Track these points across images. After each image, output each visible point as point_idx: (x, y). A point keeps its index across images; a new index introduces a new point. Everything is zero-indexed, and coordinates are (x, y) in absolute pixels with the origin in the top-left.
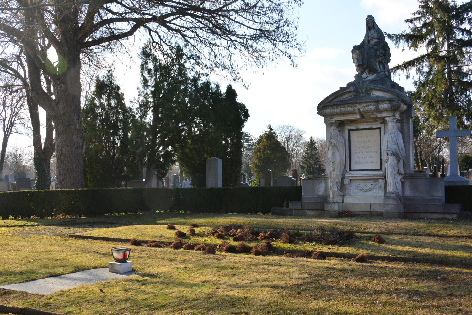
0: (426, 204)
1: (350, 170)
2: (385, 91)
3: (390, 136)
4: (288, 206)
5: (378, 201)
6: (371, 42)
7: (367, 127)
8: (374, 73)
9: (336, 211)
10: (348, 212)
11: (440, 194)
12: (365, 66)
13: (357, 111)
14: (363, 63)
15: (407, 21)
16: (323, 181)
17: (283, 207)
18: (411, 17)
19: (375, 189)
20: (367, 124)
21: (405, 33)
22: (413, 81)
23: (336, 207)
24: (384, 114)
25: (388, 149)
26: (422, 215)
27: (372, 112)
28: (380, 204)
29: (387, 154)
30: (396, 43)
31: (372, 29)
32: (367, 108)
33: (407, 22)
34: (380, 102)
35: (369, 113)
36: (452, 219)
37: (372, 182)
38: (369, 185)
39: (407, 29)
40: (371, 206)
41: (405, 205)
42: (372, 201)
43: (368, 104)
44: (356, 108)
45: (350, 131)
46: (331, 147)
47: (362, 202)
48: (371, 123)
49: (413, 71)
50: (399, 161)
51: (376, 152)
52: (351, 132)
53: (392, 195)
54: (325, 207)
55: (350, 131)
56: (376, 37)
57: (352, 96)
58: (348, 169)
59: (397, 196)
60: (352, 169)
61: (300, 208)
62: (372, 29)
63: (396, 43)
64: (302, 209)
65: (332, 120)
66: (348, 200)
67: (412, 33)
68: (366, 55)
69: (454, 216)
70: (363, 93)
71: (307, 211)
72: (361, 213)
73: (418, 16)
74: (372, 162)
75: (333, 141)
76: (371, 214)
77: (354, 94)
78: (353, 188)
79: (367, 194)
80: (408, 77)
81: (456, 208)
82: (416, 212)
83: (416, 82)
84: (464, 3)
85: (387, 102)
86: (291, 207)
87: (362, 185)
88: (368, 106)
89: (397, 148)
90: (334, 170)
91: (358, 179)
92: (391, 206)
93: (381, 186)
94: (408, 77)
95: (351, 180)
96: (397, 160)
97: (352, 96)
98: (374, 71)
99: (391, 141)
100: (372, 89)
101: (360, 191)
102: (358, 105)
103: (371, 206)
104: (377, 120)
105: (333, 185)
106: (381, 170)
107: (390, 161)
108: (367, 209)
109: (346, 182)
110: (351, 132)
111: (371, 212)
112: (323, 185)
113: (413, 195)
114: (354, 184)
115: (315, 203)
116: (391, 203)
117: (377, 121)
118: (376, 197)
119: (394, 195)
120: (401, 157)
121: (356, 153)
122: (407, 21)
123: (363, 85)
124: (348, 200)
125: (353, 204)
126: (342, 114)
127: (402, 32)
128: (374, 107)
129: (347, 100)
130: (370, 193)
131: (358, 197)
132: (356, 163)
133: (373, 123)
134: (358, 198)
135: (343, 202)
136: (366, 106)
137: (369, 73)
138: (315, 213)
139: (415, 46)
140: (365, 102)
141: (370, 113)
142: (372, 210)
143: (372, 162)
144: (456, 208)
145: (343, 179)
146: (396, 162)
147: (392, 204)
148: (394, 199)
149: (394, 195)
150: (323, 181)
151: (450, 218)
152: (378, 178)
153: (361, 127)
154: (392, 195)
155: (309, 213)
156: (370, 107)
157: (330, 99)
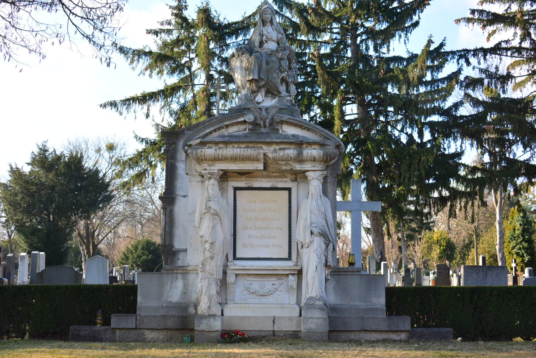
0: (362, 317)
1: (235, 258)
2: (305, 128)
3: (314, 203)
4: (107, 322)
5: (286, 313)
6: (265, 45)
7: (268, 185)
8: (274, 96)
9: (217, 331)
10: (237, 332)
11: (381, 301)
12: (263, 83)
13: (262, 156)
14: (259, 77)
15: (149, 32)
16: (180, 276)
17: (95, 324)
18: (157, 27)
19: (278, 293)
20: (268, 179)
21: (147, 50)
22: (154, 123)
23: (217, 325)
24: (307, 166)
25: (313, 225)
26: (353, 336)
27: (287, 160)
28: (290, 319)
29: (312, 233)
30: (132, 62)
31: (268, 24)
32: (281, 153)
33: (149, 33)
34: (305, 146)
35: (280, 162)
36: (400, 341)
37: (274, 280)
38: (268, 284)
39: (153, 44)
40: (274, 322)
41: (331, 320)
42: (277, 313)
43: (283, 146)
44: (262, 151)
46: (207, 215)
47: (259, 314)
48: (275, 179)
49: (156, 107)
50: (327, 246)
51: (281, 229)
52: (238, 192)
53: (318, 303)
54: (196, 325)
55: (236, 189)
56: (275, 38)
57: (245, 130)
58: (231, 257)
59: (325, 304)
60: (238, 256)
61: (134, 326)
62: (268, 24)
63: (132, 62)
64: (136, 328)
65: (212, 168)
66: (231, 311)
67: (159, 52)
68: (264, 63)
69: (403, 336)
70: (265, 126)
71: (147, 332)
72: (256, 334)
73: (167, 27)
74: (273, 245)
75: (212, 204)
76: (274, 335)
77: (250, 127)
78: (238, 289)
79: (264, 300)
80: (148, 116)
81: (405, 323)
82: (345, 331)
83: (157, 125)
84: (230, 22)
85: (316, 147)
86: (114, 324)
87: (256, 284)
88: (284, 149)
89: (325, 224)
90: (212, 258)
91: (249, 275)
92: (316, 321)
93: (291, 287)
94: (148, 116)
95: (236, 275)
96: (325, 243)
97: (245, 130)
98: (276, 93)
99: (316, 212)
100: (282, 122)
101: (252, 296)
102: (264, 147)
103: (274, 322)
104: (286, 174)
105: (209, 284)
106: (289, 258)
107: (315, 245)
108: (268, 327)
109: (231, 278)
110: (238, 192)
111: (274, 331)
112: (180, 283)
113: (340, 303)
114: (243, 282)
115: (164, 316)
116: (316, 316)
117: (286, 177)
118: (282, 306)
119: (321, 303)
120: (331, 239)
121: (245, 228)
122: (149, 32)
123: (267, 113)
124: (231, 311)
125: (243, 318)
126: (234, 159)
127: (142, 48)
128: (295, 152)
129: (236, 136)
130: (270, 299)
131: (251, 305)
132: (244, 246)
133: (280, 179)
134: (248, 308)
135: (222, 315)
136: (280, 149)
137: (266, 96)
138: (161, 335)
139: (454, 58)
140: (278, 143)
141: (283, 163)
142: (276, 329)
143: (273, 245)
144: (405, 323)
145: (225, 273)
146: (324, 246)
147: (318, 318)
148: (322, 309)
149: (321, 303)
150: (180, 276)
151: (397, 338)
152: (288, 272)
154: (318, 303)
155: (149, 335)
156: (287, 152)
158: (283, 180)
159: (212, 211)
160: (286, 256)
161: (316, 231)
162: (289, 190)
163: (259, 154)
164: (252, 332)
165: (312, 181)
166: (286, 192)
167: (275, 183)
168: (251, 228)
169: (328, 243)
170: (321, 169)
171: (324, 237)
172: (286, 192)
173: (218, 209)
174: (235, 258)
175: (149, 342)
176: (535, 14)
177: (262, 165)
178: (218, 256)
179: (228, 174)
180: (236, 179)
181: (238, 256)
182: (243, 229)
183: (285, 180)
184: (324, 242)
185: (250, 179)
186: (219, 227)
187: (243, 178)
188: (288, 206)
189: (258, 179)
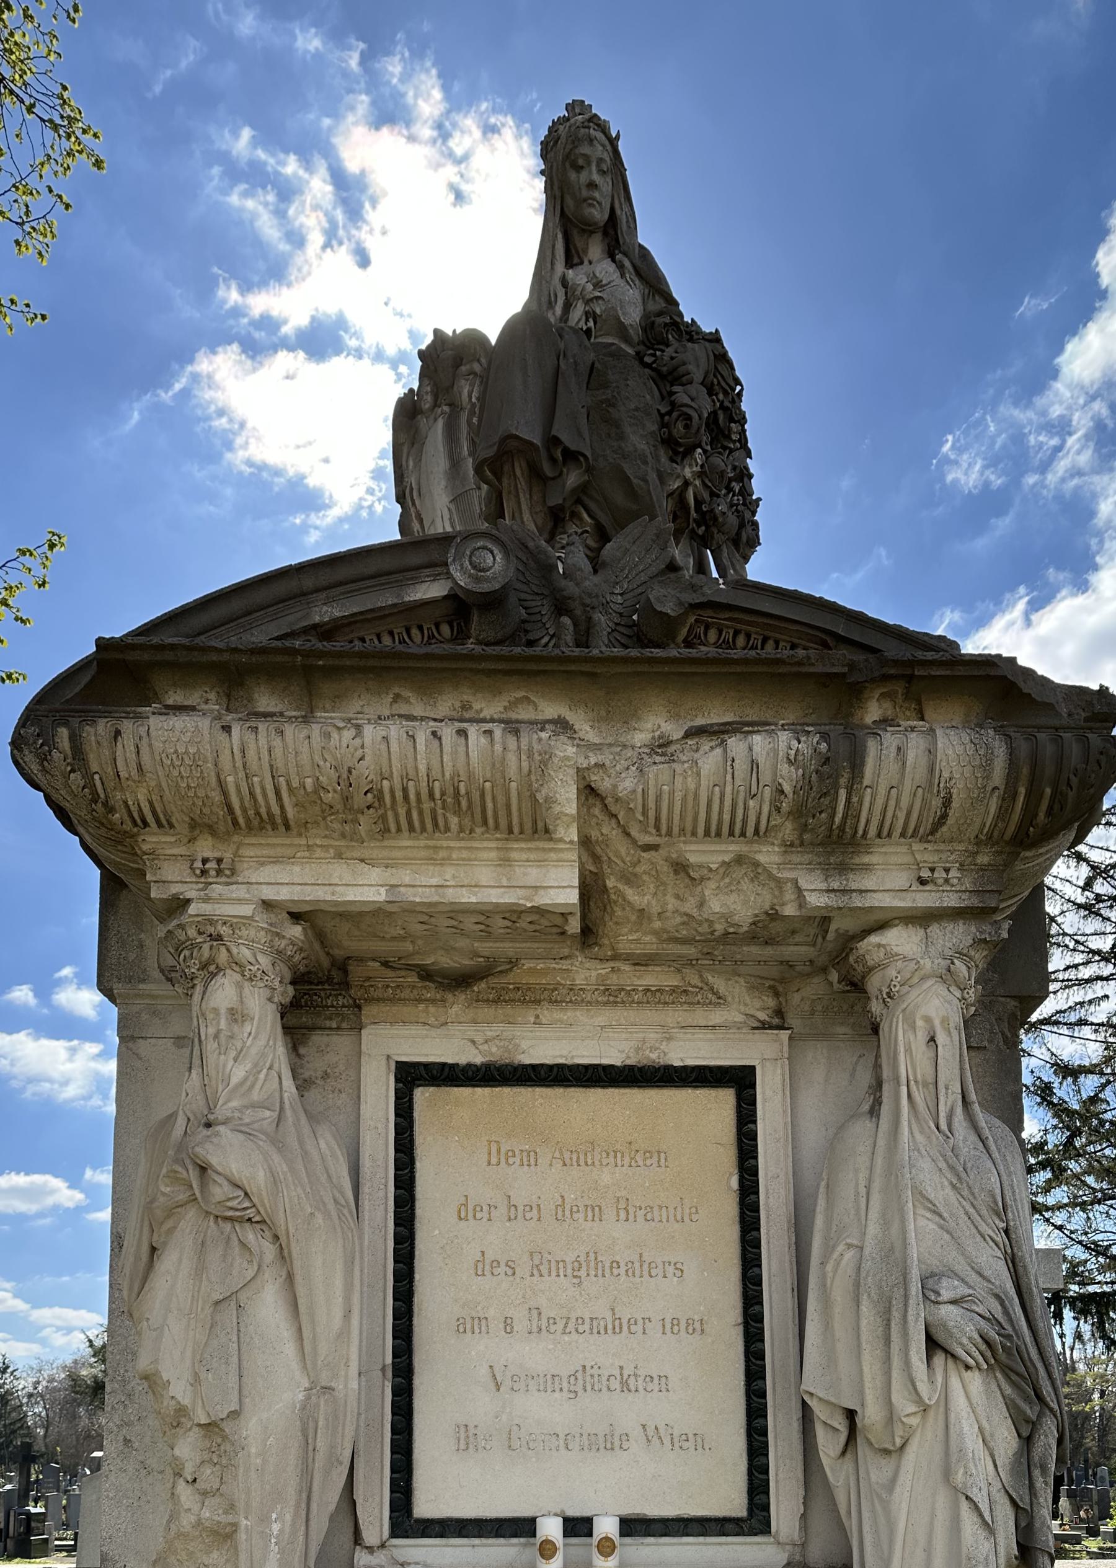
1: (405, 1522)
29: (933, 1344)
31: (595, 249)
45: (411, 1077)
48: (651, 1015)
51: (697, 1327)
52: (422, 1096)
55: (411, 1077)
60: (424, 1507)
74: (652, 1435)
110: (422, 1096)
121: (470, 1324)
133: (673, 1016)
143: (652, 1435)
153: (542, 1046)
157: (324, 612)
158: (700, 1016)
159: (220, 1191)
160: (735, 1504)
161: (962, 1328)
162: (740, 1081)
163: (543, 763)
164: (626, 208)
165: (913, 996)
166: (724, 1100)
167: (652, 1036)
168: (508, 1325)
169: (1031, 1413)
170: (967, 901)
171: (1007, 1371)
172: (724, 1100)
173: (261, 1176)
174: (405, 1522)
175: (367, 1548)
176: (1115, 900)
177: (572, 877)
178: (265, 1520)
179: (356, 972)
180: (406, 1010)
181: (424, 1507)
182: (461, 1327)
183: (717, 1016)
184: (1010, 1405)
185: (501, 1011)
186: (268, 1307)
187: (457, 1005)
188: (734, 1182)
189: (547, 1014)
